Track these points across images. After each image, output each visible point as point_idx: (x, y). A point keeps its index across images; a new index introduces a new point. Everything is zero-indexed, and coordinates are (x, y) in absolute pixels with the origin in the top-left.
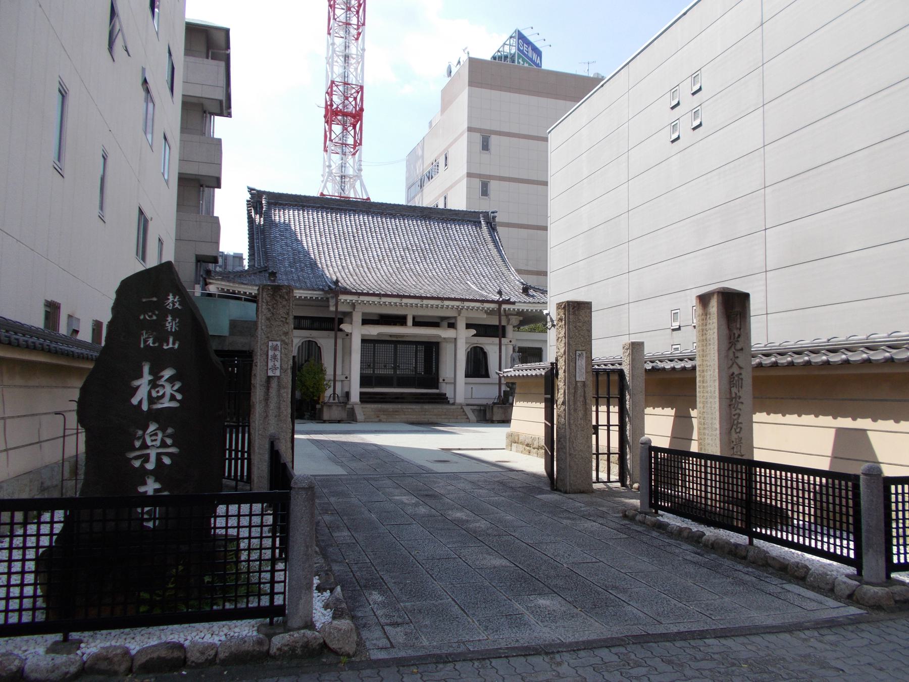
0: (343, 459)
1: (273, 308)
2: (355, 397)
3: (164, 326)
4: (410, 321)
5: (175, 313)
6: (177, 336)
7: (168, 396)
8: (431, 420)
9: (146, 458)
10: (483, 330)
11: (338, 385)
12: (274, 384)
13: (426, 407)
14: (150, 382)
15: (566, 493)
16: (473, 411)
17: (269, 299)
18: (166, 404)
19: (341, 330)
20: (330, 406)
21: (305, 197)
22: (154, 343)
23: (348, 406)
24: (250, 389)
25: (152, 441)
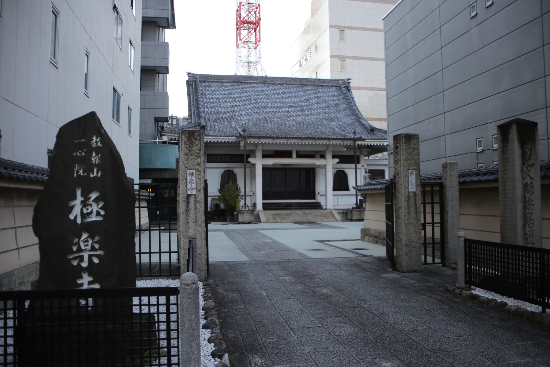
0: (248, 250)
1: (190, 147)
2: (259, 207)
3: (91, 160)
4: (294, 155)
5: (98, 150)
6: (99, 167)
7: (95, 212)
8: (310, 220)
9: (81, 259)
10: (344, 159)
11: (248, 199)
12: (192, 199)
13: (307, 211)
14: (82, 202)
15: (403, 272)
16: (339, 214)
17: (186, 140)
18: (94, 218)
19: (249, 162)
20: (242, 212)
21: (223, 76)
22: (83, 173)
23: (255, 213)
24: (176, 204)
25: (85, 246)
